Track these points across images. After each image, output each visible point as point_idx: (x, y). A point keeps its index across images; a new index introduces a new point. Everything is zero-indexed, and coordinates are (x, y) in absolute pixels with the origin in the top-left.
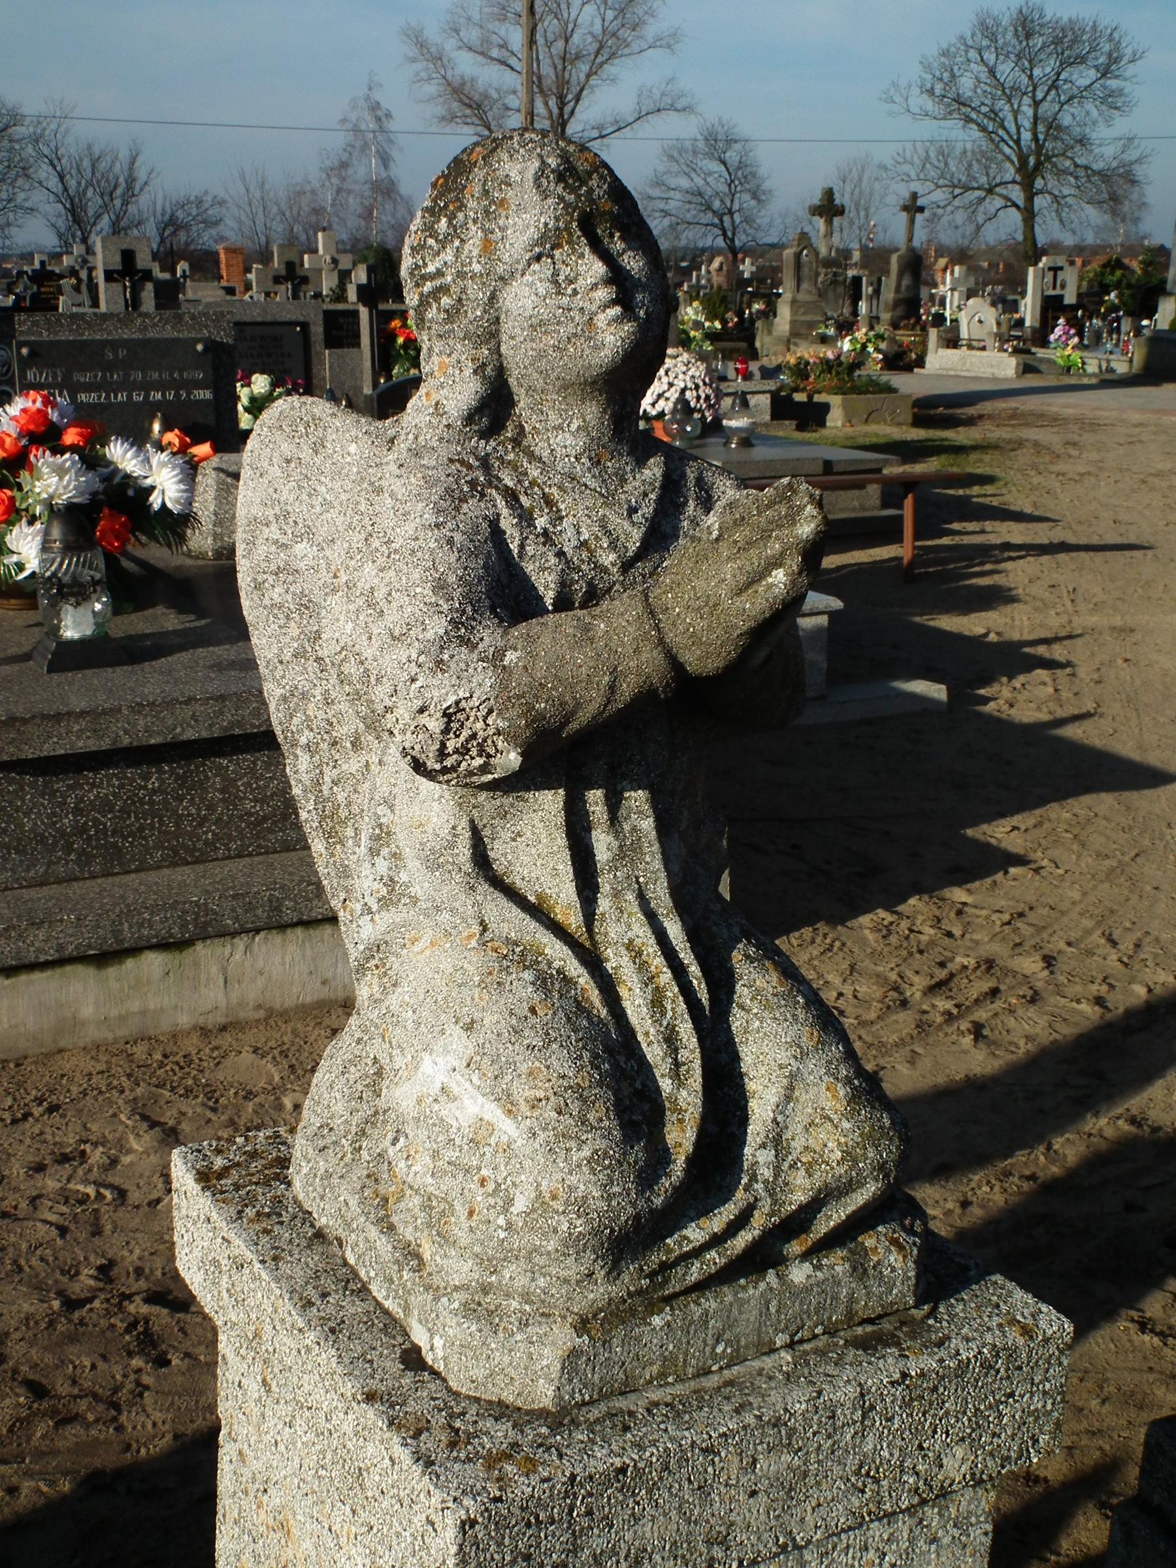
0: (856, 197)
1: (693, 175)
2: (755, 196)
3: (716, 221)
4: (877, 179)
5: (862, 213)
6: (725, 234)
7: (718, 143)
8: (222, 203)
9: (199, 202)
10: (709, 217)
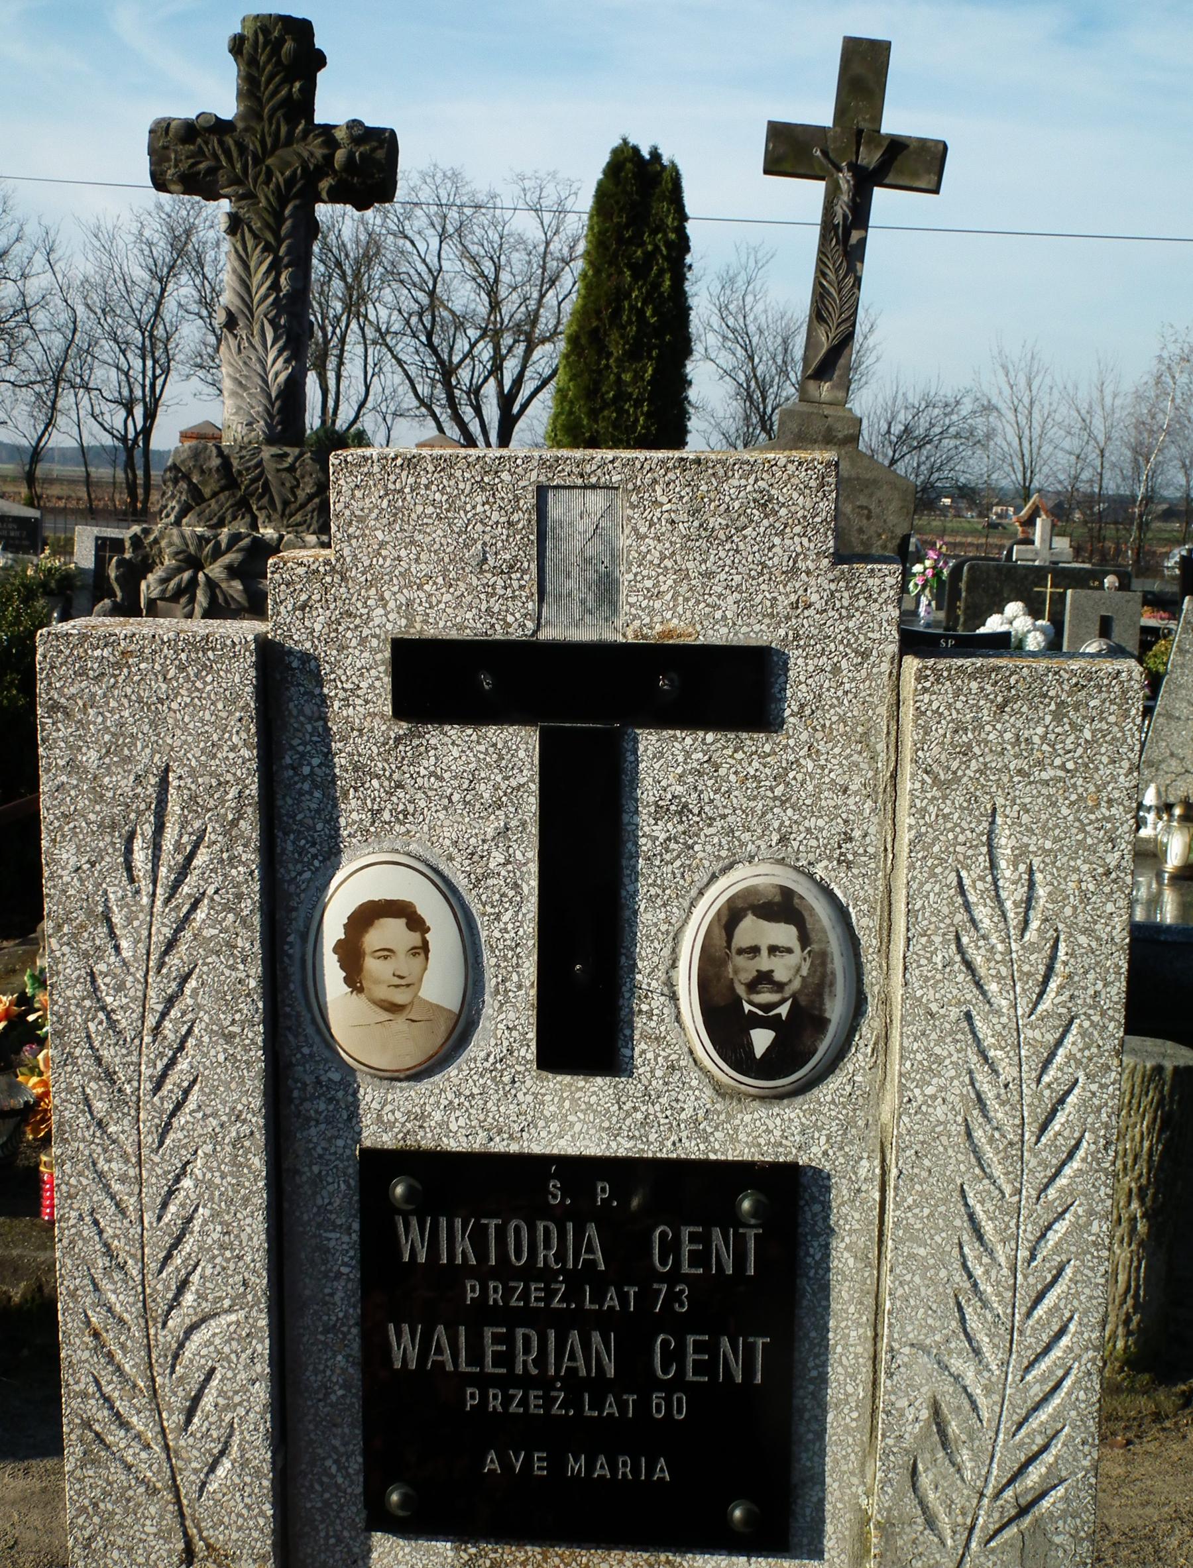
8: (988, 408)
9: (950, 407)
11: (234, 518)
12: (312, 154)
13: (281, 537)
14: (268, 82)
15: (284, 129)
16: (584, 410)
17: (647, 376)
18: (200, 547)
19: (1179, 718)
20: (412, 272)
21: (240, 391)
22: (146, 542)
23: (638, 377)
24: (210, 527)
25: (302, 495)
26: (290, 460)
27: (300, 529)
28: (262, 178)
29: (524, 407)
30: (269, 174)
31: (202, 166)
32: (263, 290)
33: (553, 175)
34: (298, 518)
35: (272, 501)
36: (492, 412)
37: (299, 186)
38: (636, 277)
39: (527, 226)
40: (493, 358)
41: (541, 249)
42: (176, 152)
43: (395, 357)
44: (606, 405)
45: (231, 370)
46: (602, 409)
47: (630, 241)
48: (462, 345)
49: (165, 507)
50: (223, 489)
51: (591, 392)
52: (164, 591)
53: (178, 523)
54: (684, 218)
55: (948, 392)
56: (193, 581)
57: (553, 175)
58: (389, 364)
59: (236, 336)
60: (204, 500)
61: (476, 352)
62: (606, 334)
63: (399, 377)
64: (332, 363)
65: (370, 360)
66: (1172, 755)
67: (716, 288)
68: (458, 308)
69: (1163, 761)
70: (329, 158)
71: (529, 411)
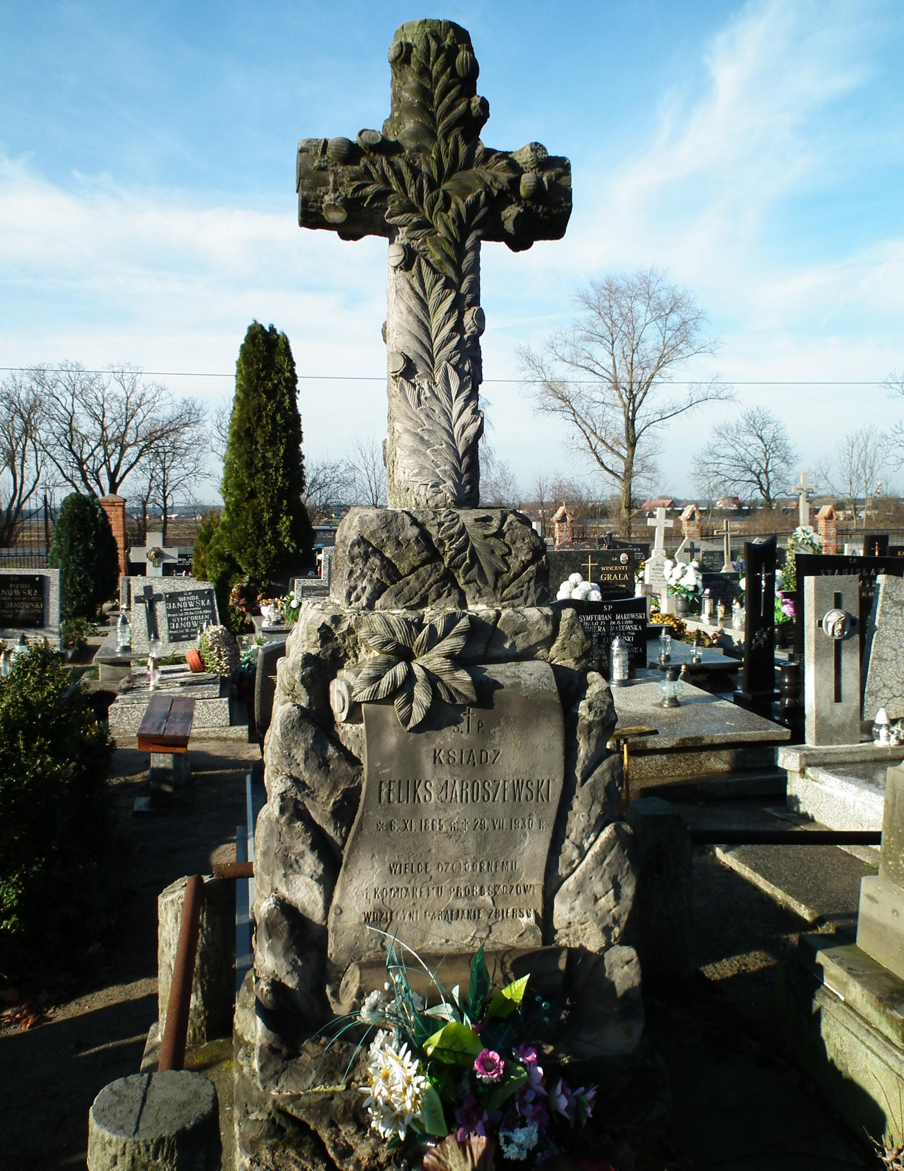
0: (862, 458)
1: (737, 446)
2: (784, 459)
3: (755, 479)
4: (879, 445)
5: (868, 470)
6: (761, 488)
7: (756, 425)
8: (353, 468)
9: (335, 468)
10: (749, 476)
11: (439, 596)
12: (495, 178)
13: (498, 614)
14: (443, 95)
15: (463, 150)
16: (245, 475)
17: (281, 454)
18: (410, 635)
19: (886, 660)
20: (59, 414)
21: (422, 448)
22: (337, 633)
23: (275, 454)
24: (411, 608)
25: (515, 564)
26: (495, 523)
27: (516, 602)
28: (439, 204)
29: (122, 479)
30: (447, 200)
31: (370, 189)
32: (445, 331)
33: (128, 364)
34: (512, 589)
35: (481, 571)
36: (105, 482)
37: (482, 213)
38: (269, 398)
39: (115, 388)
40: (105, 456)
41: (125, 401)
42: (336, 174)
43: (51, 457)
44: (258, 471)
45: (409, 425)
46: (256, 474)
47: (264, 379)
48: (87, 450)
49: (355, 588)
50: (424, 563)
51: (249, 464)
52: (375, 692)
53: (370, 606)
54: (293, 364)
55: (333, 460)
56: (410, 677)
57: (128, 364)
58: (48, 461)
59: (414, 386)
60: (400, 577)
61: (95, 453)
62: (254, 431)
63: (55, 467)
64: (18, 462)
65: (39, 458)
66: (884, 686)
67: (215, 418)
68: (83, 431)
69: (879, 690)
70: (515, 183)
71: (125, 480)
